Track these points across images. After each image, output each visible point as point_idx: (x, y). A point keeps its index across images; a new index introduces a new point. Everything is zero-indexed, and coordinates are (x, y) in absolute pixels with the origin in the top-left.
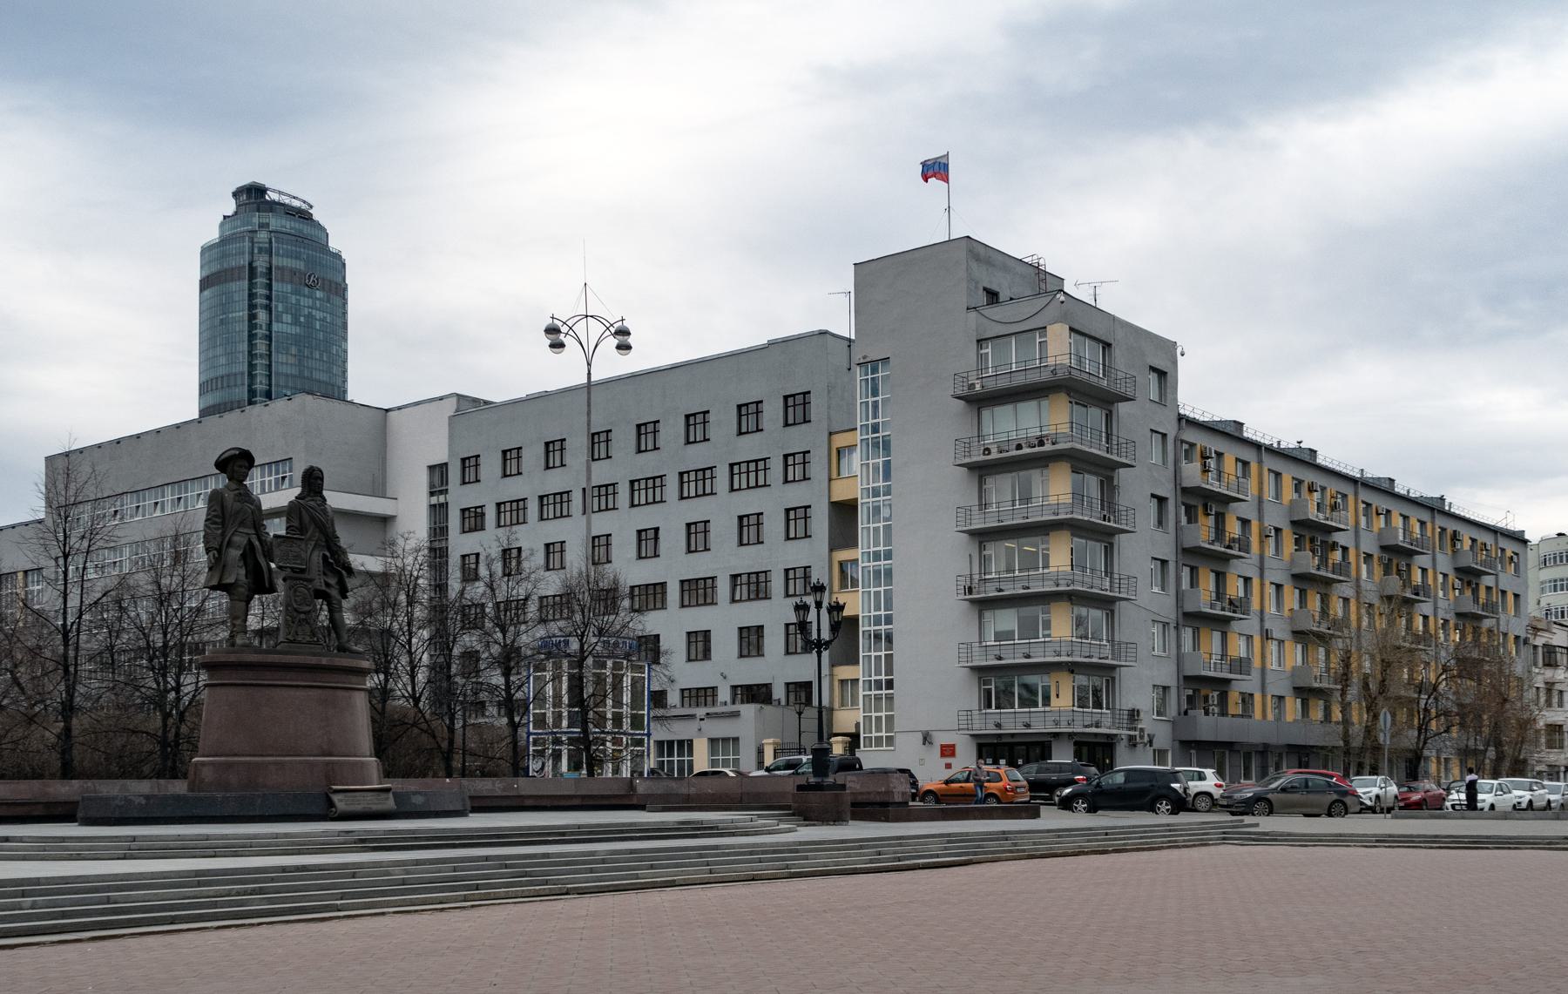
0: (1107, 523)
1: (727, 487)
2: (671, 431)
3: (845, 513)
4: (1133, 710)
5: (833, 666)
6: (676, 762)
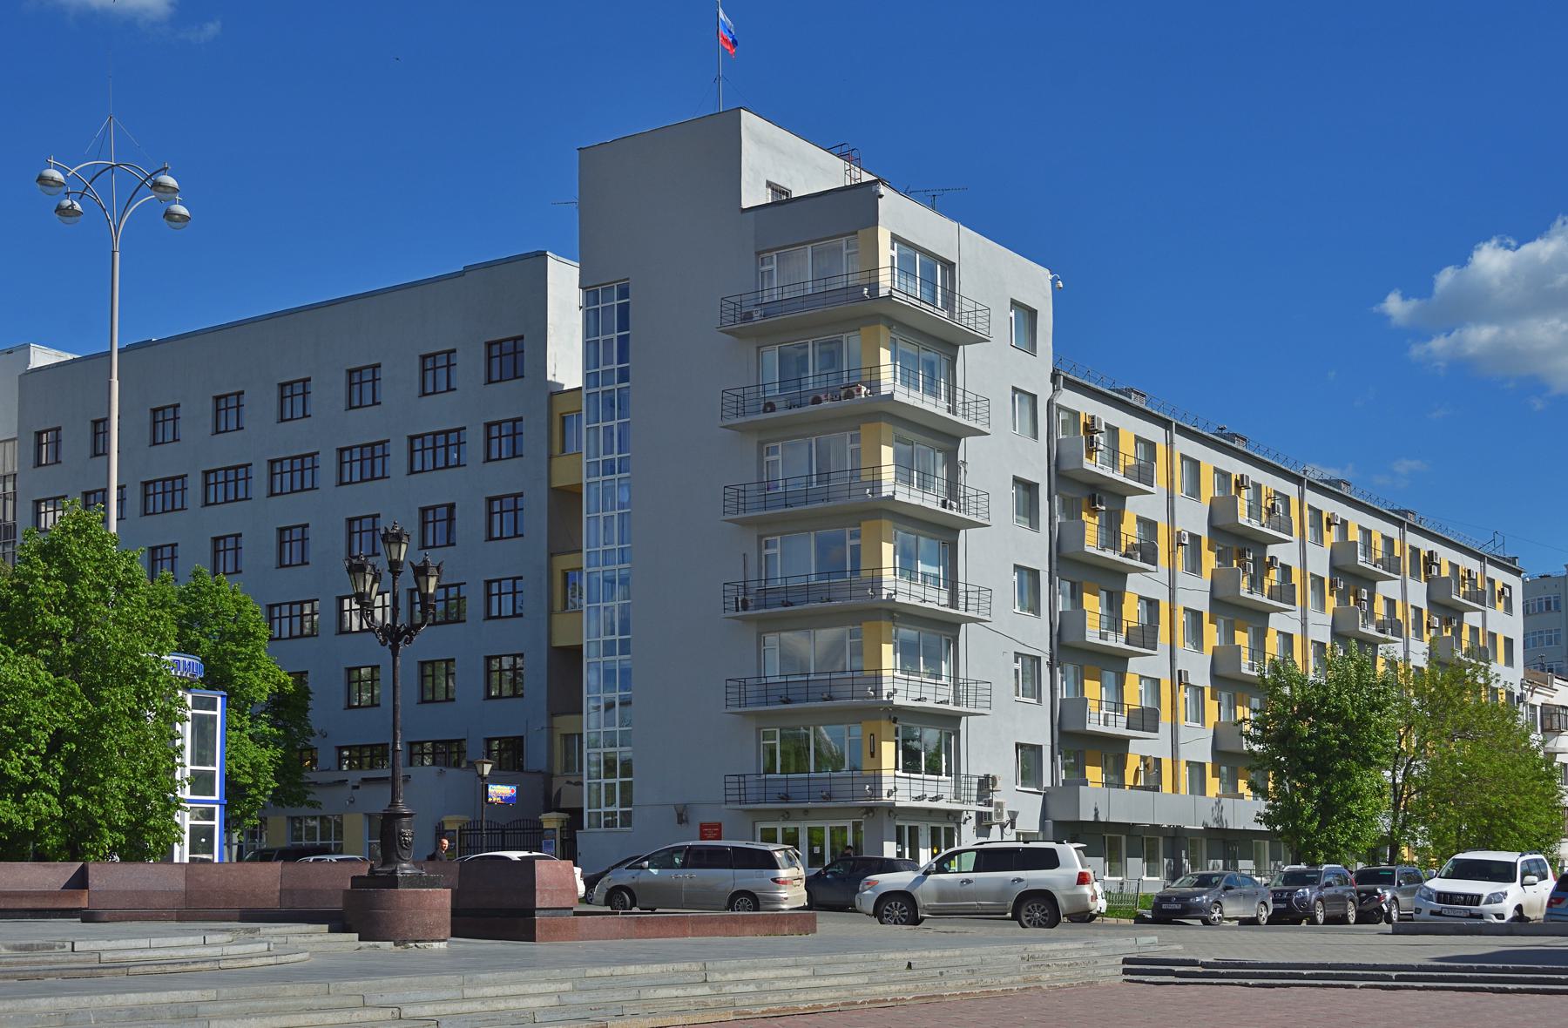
0: (947, 511)
1: (405, 468)
2: (328, 393)
3: (566, 500)
4: (987, 777)
5: (553, 715)
6: (318, 838)
